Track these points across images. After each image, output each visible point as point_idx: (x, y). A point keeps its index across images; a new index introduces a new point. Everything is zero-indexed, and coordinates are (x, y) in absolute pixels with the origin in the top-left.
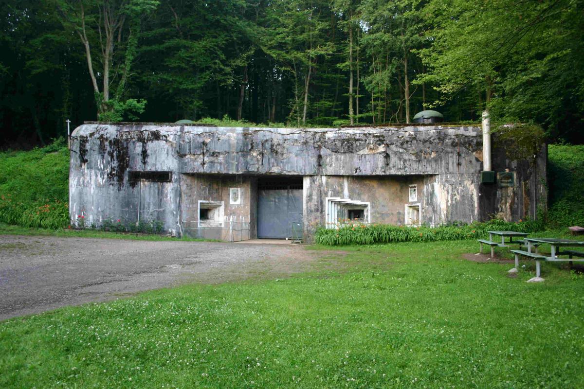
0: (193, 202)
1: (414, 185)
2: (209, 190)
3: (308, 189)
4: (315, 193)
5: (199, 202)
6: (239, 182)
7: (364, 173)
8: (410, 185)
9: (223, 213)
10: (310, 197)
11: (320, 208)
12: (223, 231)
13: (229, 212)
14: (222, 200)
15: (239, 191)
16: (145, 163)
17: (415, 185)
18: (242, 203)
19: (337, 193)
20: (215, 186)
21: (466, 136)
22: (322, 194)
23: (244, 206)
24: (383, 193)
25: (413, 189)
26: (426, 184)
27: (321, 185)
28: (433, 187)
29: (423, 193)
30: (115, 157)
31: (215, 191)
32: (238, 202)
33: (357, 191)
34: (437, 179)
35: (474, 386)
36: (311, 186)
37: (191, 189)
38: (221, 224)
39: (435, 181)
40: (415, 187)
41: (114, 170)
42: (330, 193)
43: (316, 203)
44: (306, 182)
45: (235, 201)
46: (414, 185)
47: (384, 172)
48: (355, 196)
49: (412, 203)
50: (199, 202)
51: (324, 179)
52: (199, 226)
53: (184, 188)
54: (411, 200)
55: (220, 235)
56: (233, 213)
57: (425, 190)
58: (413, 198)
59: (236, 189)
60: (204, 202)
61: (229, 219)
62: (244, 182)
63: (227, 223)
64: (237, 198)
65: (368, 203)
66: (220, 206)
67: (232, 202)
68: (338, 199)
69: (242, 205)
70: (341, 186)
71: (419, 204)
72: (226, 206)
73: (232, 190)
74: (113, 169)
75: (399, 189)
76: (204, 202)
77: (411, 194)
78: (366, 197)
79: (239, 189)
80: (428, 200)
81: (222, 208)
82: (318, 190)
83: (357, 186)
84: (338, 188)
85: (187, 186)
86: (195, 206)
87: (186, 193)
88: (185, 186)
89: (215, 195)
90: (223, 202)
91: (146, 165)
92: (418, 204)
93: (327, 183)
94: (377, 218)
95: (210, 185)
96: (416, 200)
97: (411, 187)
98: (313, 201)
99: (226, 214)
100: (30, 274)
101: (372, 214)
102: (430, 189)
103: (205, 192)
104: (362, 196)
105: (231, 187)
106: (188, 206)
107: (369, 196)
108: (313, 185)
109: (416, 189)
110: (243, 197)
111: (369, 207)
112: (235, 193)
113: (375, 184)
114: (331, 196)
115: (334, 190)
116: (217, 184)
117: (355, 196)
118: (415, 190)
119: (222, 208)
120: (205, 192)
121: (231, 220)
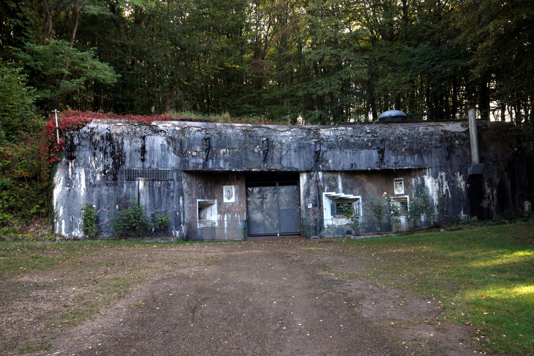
0: (193, 202)
1: (399, 179)
2: (205, 189)
3: (305, 186)
4: (312, 188)
5: (198, 200)
6: (233, 180)
7: (357, 169)
8: (395, 179)
9: (216, 212)
10: (308, 193)
11: (318, 203)
12: (217, 231)
13: (223, 209)
14: (214, 199)
15: (233, 189)
16: (143, 160)
17: (402, 178)
18: (237, 200)
19: (333, 188)
20: (209, 184)
21: (452, 132)
22: (319, 190)
23: (240, 204)
24: (371, 187)
25: (399, 182)
26: (414, 177)
27: (317, 181)
28: (423, 180)
29: (412, 186)
30: (109, 155)
31: (209, 190)
32: (233, 200)
33: (350, 186)
34: (427, 173)
35: (496, 352)
36: (308, 182)
37: (191, 187)
38: (215, 223)
39: (426, 175)
40: (402, 180)
41: (108, 168)
42: (326, 188)
43: (313, 199)
44: (303, 179)
45: (229, 199)
46: (399, 179)
47: (379, 167)
48: (348, 190)
49: (398, 195)
50: (198, 200)
51: (320, 174)
52: (198, 226)
53: (185, 186)
54: (396, 193)
55: (215, 234)
56: (228, 211)
57: (413, 182)
58: (399, 191)
59: (230, 186)
60: (201, 200)
61: (223, 218)
62: (238, 179)
63: (221, 222)
64: (232, 195)
65: (359, 197)
66: (213, 204)
67: (225, 200)
68: (334, 194)
69: (237, 203)
70: (335, 180)
71: (407, 197)
72: (220, 203)
73: (225, 188)
74: (106, 167)
75: (384, 183)
76: (201, 200)
77: (396, 187)
78: (357, 191)
79: (233, 187)
80: (417, 192)
81: (215, 207)
82: (315, 186)
83: (349, 181)
84: (333, 183)
85: (188, 185)
86: (194, 205)
87: (187, 192)
88: (186, 184)
89: (209, 193)
90: (216, 201)
91: (145, 163)
92: (405, 196)
93: (323, 178)
94: (367, 211)
95: (205, 183)
96: (403, 192)
97: (396, 181)
98: (311, 196)
99: (219, 212)
100: (429, 208)
101: (363, 207)
102: (419, 182)
103: (202, 190)
104: (354, 191)
105: (223, 185)
106: (189, 205)
107: (360, 190)
108: (310, 181)
109: (403, 182)
110: (238, 194)
111: (361, 201)
112: (229, 191)
113: (364, 178)
114: (328, 192)
115: (330, 186)
116: (211, 182)
117: (348, 190)
118: (401, 183)
119: (215, 207)
120: (202, 190)
121: (225, 219)
